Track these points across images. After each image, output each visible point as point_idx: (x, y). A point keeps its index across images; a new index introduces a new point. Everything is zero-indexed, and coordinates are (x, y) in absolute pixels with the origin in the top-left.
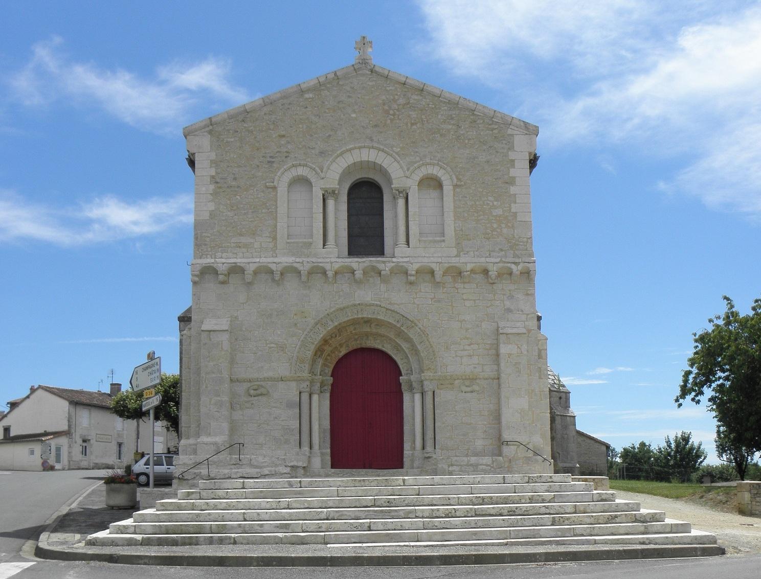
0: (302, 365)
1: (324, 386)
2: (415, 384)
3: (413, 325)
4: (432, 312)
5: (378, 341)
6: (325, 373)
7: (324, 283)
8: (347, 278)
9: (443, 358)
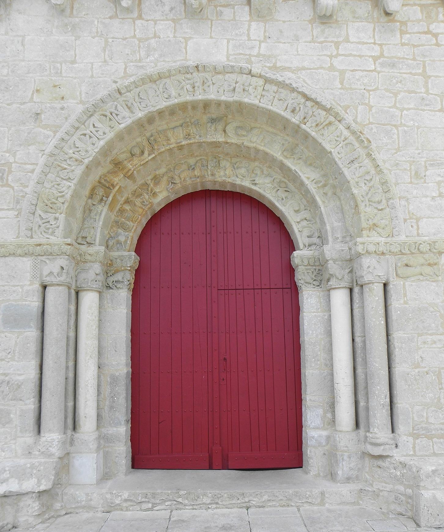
0: (50, 217)
1: (117, 272)
2: (333, 268)
3: (332, 119)
4: (377, 89)
5: (243, 171)
6: (119, 242)
7: (111, 18)
8: (167, 8)
9: (407, 200)
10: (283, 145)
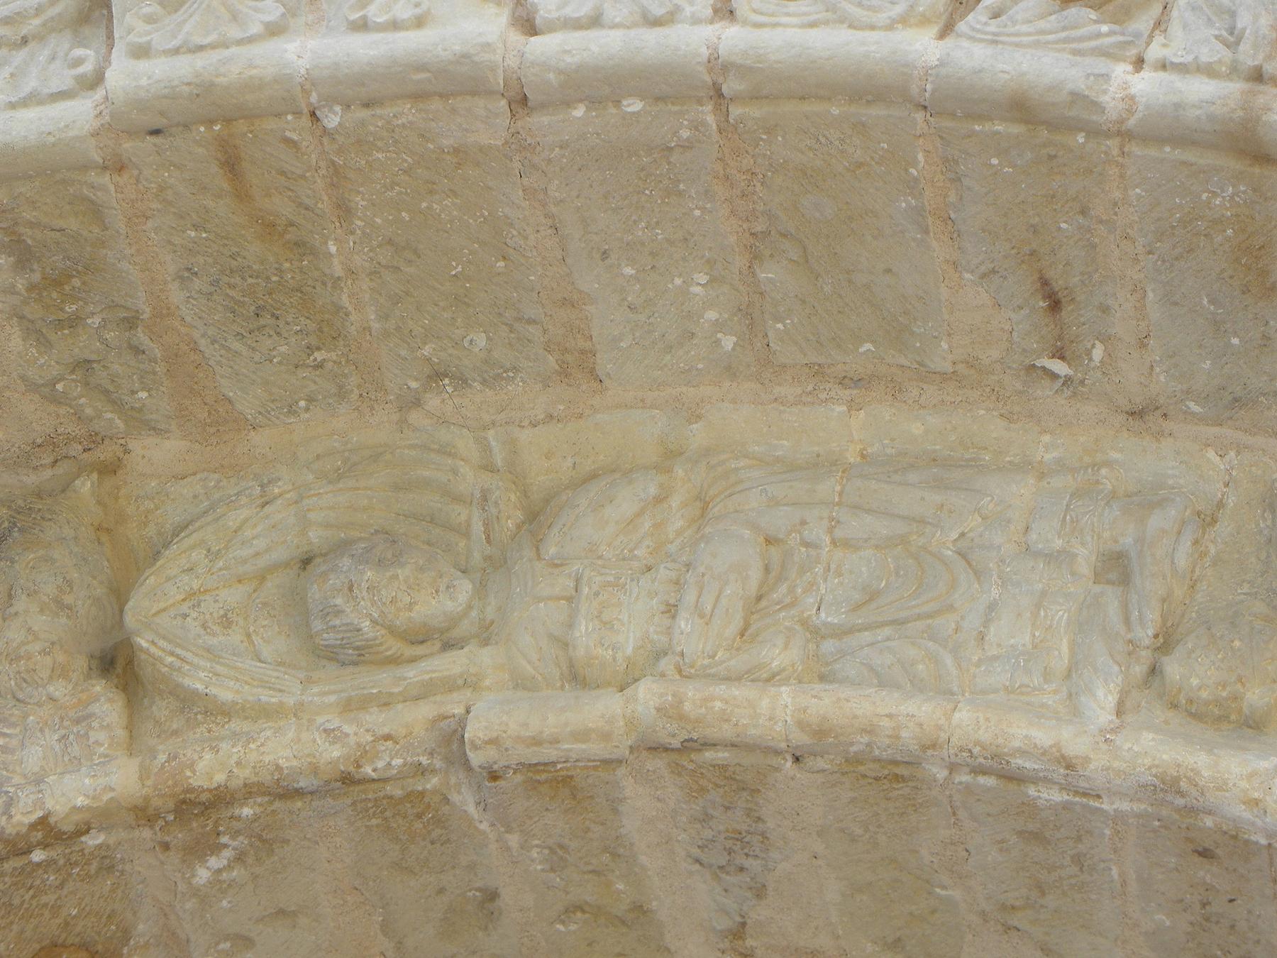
10: (1125, 580)
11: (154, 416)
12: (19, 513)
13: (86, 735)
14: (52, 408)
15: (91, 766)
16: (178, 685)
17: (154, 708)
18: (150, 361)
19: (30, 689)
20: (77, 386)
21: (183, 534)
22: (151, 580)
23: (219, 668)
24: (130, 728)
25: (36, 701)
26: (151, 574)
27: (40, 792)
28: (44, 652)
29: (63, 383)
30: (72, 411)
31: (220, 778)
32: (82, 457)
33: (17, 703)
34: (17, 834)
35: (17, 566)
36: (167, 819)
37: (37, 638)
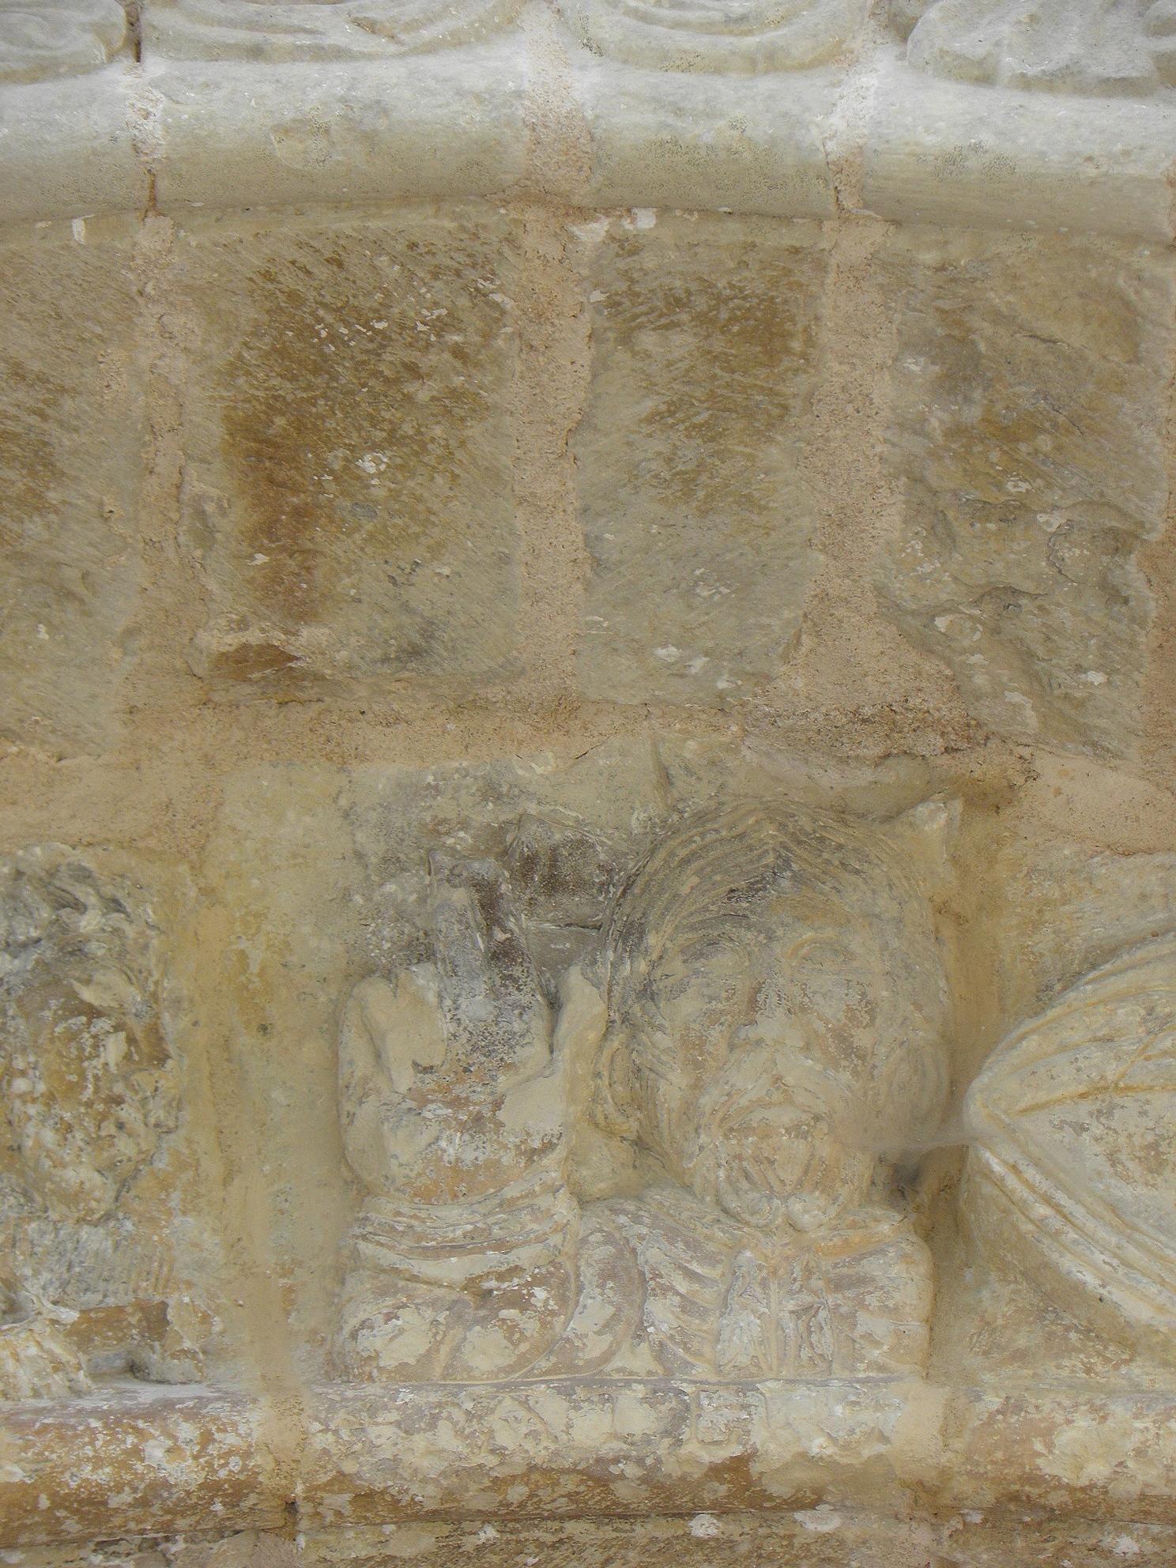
11: (1103, 723)
12: (799, 843)
13: (851, 1319)
14: (913, 657)
15: (850, 1383)
16: (1047, 1265)
17: (985, 1294)
18: (1133, 620)
19: (755, 1194)
20: (974, 630)
21: (1108, 966)
22: (1032, 1044)
23: (1132, 1252)
24: (932, 1322)
25: (762, 1222)
26: (1033, 1031)
27: (744, 1407)
28: (797, 1131)
29: (950, 617)
30: (948, 672)
31: (1097, 1470)
32: (939, 761)
33: (723, 1217)
34: (683, 1479)
35: (777, 948)
36: (969, 1519)
37: (789, 1100)
